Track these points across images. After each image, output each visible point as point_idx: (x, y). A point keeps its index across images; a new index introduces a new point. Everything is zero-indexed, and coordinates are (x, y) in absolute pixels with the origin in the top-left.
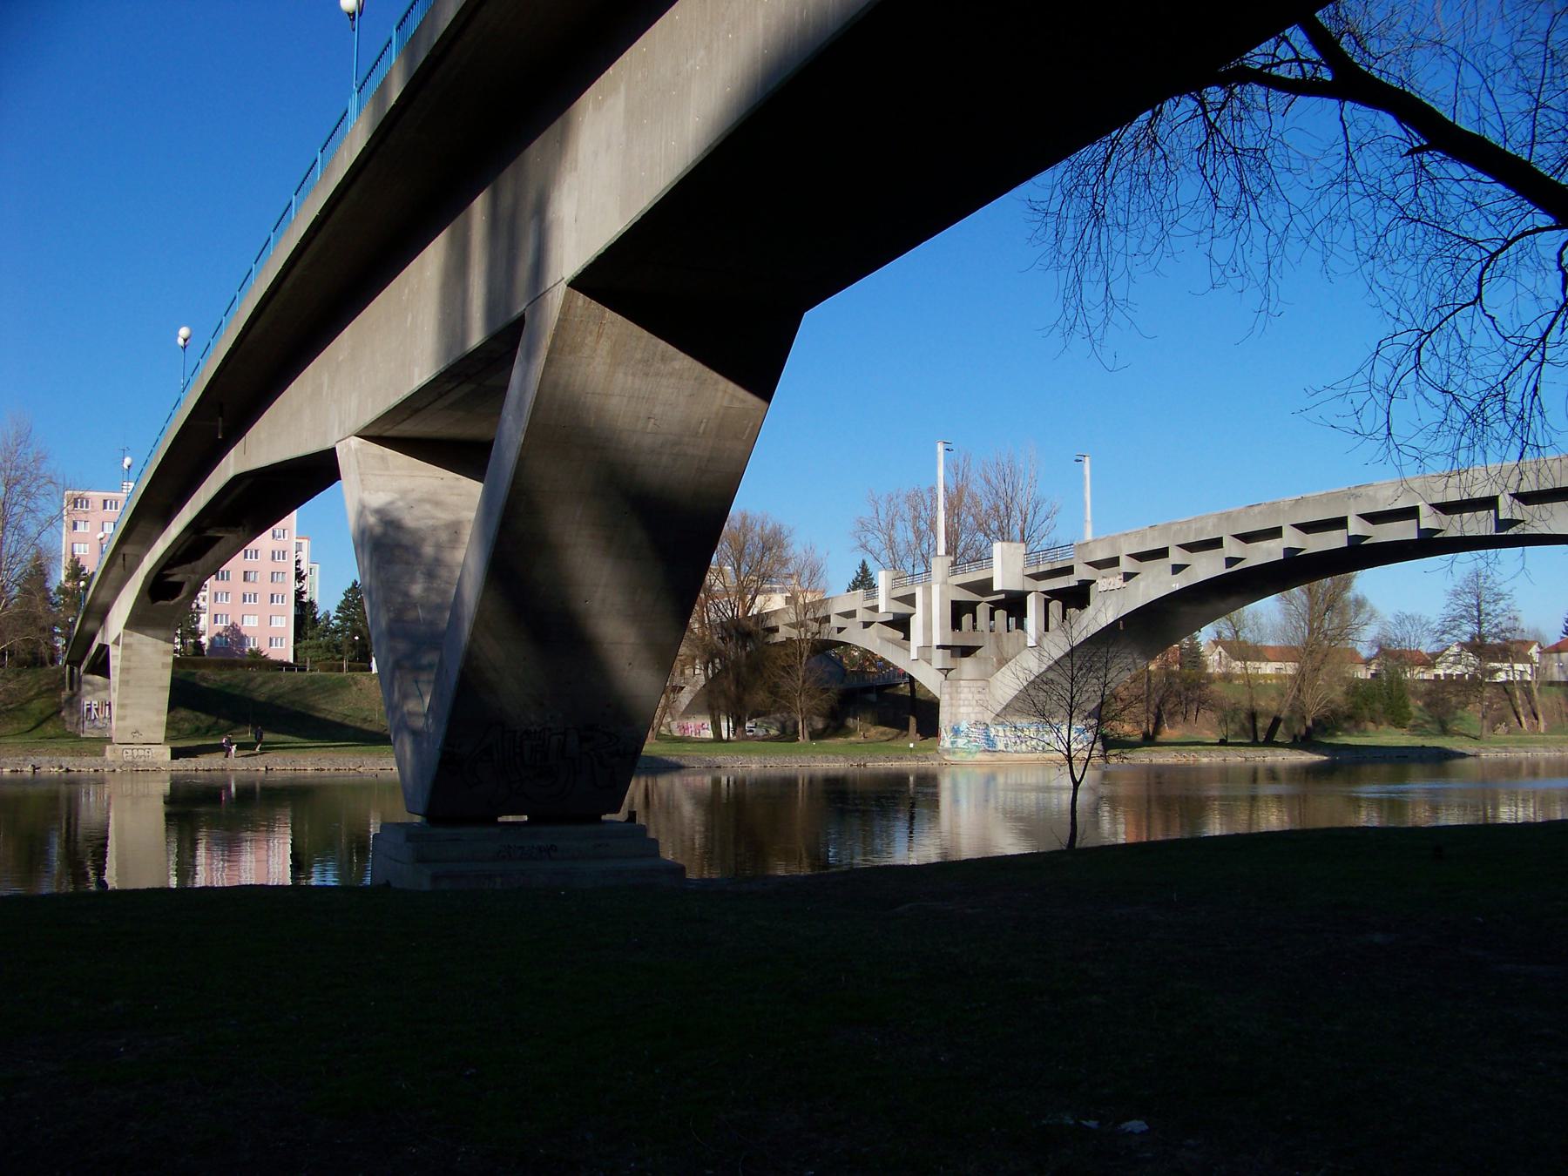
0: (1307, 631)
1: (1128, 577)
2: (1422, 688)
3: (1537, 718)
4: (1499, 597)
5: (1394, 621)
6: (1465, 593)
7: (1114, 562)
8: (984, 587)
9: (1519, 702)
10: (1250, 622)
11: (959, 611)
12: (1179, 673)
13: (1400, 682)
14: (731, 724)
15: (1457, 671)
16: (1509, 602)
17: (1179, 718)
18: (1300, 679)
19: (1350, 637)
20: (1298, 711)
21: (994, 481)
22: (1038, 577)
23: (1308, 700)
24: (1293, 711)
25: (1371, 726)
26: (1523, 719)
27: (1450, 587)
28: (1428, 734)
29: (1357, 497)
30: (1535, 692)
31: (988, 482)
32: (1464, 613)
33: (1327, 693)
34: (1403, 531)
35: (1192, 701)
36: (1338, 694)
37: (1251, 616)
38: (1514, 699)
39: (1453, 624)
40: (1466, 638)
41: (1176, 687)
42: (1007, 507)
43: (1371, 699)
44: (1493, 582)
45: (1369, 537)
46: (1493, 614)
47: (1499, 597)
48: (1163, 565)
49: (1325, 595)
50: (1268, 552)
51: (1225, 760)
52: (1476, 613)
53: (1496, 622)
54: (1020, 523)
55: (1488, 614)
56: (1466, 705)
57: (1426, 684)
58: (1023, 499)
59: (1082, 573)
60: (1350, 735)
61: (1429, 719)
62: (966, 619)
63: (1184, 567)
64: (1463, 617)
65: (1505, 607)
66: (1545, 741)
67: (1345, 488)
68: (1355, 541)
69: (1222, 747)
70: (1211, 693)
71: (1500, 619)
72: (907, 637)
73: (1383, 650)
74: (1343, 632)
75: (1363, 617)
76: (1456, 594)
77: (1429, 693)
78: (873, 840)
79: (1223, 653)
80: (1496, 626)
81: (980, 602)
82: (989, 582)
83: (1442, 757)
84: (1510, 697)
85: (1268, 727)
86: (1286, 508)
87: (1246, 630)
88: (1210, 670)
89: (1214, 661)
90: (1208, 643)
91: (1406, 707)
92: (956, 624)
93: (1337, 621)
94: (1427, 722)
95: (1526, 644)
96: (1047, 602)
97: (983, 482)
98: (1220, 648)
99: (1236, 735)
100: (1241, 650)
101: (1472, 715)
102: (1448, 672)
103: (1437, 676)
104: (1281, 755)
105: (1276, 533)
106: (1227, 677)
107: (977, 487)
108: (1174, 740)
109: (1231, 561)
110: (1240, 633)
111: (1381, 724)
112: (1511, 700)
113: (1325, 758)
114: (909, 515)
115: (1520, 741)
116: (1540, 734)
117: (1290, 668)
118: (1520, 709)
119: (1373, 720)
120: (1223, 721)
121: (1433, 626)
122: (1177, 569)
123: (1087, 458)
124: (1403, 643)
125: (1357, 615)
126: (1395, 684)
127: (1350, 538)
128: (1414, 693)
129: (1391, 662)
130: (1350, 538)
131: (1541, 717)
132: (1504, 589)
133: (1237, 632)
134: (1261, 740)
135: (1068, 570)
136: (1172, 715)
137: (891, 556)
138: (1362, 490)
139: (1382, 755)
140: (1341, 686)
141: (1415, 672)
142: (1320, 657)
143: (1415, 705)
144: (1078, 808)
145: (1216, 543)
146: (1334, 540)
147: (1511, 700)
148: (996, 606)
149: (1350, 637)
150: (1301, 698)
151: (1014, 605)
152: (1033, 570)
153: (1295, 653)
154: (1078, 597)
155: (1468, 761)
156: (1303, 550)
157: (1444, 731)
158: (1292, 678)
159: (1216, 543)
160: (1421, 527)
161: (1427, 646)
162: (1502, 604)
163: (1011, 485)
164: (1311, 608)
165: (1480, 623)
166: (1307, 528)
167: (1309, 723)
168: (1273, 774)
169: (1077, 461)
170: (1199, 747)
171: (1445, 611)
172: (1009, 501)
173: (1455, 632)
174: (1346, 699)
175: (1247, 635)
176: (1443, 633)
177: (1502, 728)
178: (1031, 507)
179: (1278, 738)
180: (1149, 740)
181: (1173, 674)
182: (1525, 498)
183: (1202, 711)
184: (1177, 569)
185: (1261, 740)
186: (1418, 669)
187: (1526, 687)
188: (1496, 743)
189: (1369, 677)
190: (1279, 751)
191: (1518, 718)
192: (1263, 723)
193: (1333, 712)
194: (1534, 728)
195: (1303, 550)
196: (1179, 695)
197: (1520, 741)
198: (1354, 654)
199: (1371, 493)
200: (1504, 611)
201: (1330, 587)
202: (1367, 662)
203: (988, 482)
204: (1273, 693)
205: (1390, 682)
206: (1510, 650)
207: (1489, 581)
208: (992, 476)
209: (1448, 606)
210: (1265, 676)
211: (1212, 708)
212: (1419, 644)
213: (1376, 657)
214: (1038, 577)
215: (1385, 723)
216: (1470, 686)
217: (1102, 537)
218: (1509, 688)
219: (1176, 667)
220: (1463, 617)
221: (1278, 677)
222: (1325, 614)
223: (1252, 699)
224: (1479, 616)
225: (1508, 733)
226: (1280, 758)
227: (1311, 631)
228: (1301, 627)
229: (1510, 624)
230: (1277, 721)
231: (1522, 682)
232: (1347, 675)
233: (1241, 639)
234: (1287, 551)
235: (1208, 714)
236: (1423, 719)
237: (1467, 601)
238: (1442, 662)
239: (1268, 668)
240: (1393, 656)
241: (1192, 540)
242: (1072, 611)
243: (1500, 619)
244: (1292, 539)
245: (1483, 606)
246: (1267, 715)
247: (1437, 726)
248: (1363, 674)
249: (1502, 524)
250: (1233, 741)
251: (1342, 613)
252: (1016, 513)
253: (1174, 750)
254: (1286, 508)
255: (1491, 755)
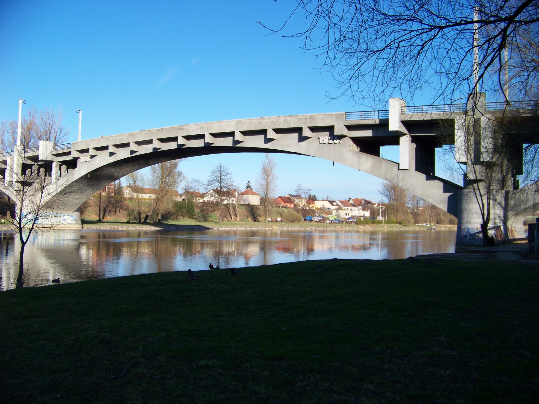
0: (160, 183)
1: (92, 156)
2: (199, 205)
3: (237, 216)
4: (228, 174)
5: (191, 181)
6: (216, 172)
7: (87, 151)
8: (35, 159)
9: (231, 211)
10: (140, 178)
11: (25, 167)
12: (113, 196)
13: (192, 203)
14: (523, 242)
15: (212, 199)
16: (231, 176)
17: (113, 213)
18: (157, 201)
19: (176, 185)
20: (156, 212)
21: (45, 119)
22: (57, 155)
23: (160, 208)
24: (153, 212)
25: (181, 217)
26: (232, 216)
27: (211, 170)
28: (200, 221)
29: (182, 129)
30: (237, 208)
31: (42, 119)
32: (215, 179)
33: (166, 206)
34: (198, 143)
35: (118, 207)
36: (170, 206)
37: (140, 176)
38: (229, 210)
39: (211, 182)
40: (215, 188)
41: (112, 202)
42: (49, 130)
43: (182, 208)
44: (226, 168)
45: (186, 145)
46: (225, 180)
47: (228, 174)
48: (106, 153)
49: (167, 169)
50: (147, 149)
51: (128, 229)
52: (219, 179)
53: (226, 182)
54: (54, 136)
55: (223, 180)
56: (214, 211)
57: (201, 204)
58: (55, 127)
59: (75, 154)
60: (174, 221)
61: (200, 216)
62: (28, 172)
63: (115, 153)
64: (215, 180)
65: (229, 178)
66: (240, 224)
67: (178, 126)
68: (180, 146)
69: (127, 224)
70: (125, 204)
71: (228, 182)
72: (4, 178)
73: (187, 191)
74: (173, 184)
75: (181, 178)
76: (213, 172)
77: (202, 207)
78: (495, 145)
79: (130, 190)
80: (226, 184)
81: (34, 165)
82: (37, 157)
83: (201, 229)
84: (229, 209)
85: (145, 217)
86: (155, 132)
87: (138, 181)
88: (125, 196)
89: (127, 193)
90: (125, 187)
91: (194, 211)
92: (24, 172)
93: (171, 179)
94: (200, 217)
95: (235, 191)
96: (60, 166)
97: (40, 119)
98: (129, 188)
99: (132, 220)
100: (136, 189)
101: (216, 215)
102: (209, 200)
103: (204, 201)
104: (149, 227)
105: (150, 142)
106: (131, 199)
107: (38, 122)
108: (111, 221)
109: (132, 152)
110: (136, 182)
111: (185, 217)
112: (228, 210)
113: (162, 229)
114: (10, 130)
115: (232, 224)
116: (238, 221)
117: (154, 196)
118: (232, 213)
119: (182, 216)
120: (129, 214)
121: (204, 184)
122: (112, 154)
123: (81, 112)
124: (194, 189)
125: (178, 178)
126: (190, 203)
127: (178, 145)
128: (197, 207)
129: (189, 196)
130: (178, 145)
131: (238, 216)
132: (229, 171)
133: (135, 182)
134: (142, 222)
135: (69, 153)
136: (110, 212)
137: (2, 146)
138: (184, 127)
139: (185, 228)
140: (172, 203)
141: (197, 200)
142: (165, 192)
143: (197, 210)
144: (24, 261)
145: (127, 145)
146: (173, 146)
147: (228, 210)
148: (40, 166)
149: (176, 185)
150: (157, 207)
151: (47, 166)
152: (55, 153)
153: (156, 190)
154: (72, 164)
155: (210, 230)
156: (160, 149)
157: (206, 220)
158: (154, 199)
159: (127, 145)
160: (205, 142)
161: (202, 191)
162: (228, 176)
163: (51, 121)
164: (162, 174)
165: (221, 183)
166: (162, 140)
167: (160, 217)
168: (146, 233)
169: (77, 112)
170: (119, 224)
171: (209, 178)
172: (50, 127)
173: (212, 185)
174: (173, 208)
175: (139, 184)
176: (208, 185)
177: (225, 219)
178: (59, 130)
179: (148, 221)
180: (99, 221)
181: (112, 197)
182: (245, 133)
183: (121, 211)
184: (112, 154)
185: (142, 222)
186: (198, 198)
187: (234, 206)
188: (225, 224)
189: (181, 200)
190: (148, 226)
191: (231, 216)
192: (143, 216)
193: (168, 212)
194: (236, 220)
195: (160, 149)
196: (113, 204)
197: (232, 224)
198: (176, 192)
199: (187, 128)
200: (229, 179)
201: (169, 167)
202: (181, 195)
203: (42, 119)
204: (147, 205)
205: (189, 202)
206: (229, 194)
207: (225, 168)
208: (44, 117)
209: (210, 176)
210: (144, 199)
211: (125, 210)
212: (199, 190)
213: (184, 194)
214: (57, 155)
215: (186, 217)
216: (215, 205)
217: (83, 141)
218: (228, 206)
219: (113, 195)
220: (215, 180)
221: (150, 199)
222: (167, 177)
223: (139, 206)
224: (220, 180)
225: (227, 221)
226: (149, 228)
227: (162, 183)
228: (158, 181)
229: (229, 184)
230: (147, 217)
231: (233, 204)
232: (174, 200)
233: (136, 184)
234: (154, 149)
235: (124, 212)
236: (198, 216)
237: (217, 175)
238: (207, 196)
239: (146, 196)
240: (190, 194)
241: (118, 143)
242: (70, 170)
243: (228, 182)
244: (156, 144)
245: (222, 176)
246: (145, 213)
247: (203, 219)
248: (180, 199)
249: (236, 142)
250: (132, 222)
251: (173, 177)
252: (53, 132)
253: (109, 225)
254: (155, 132)
255: (223, 229)
